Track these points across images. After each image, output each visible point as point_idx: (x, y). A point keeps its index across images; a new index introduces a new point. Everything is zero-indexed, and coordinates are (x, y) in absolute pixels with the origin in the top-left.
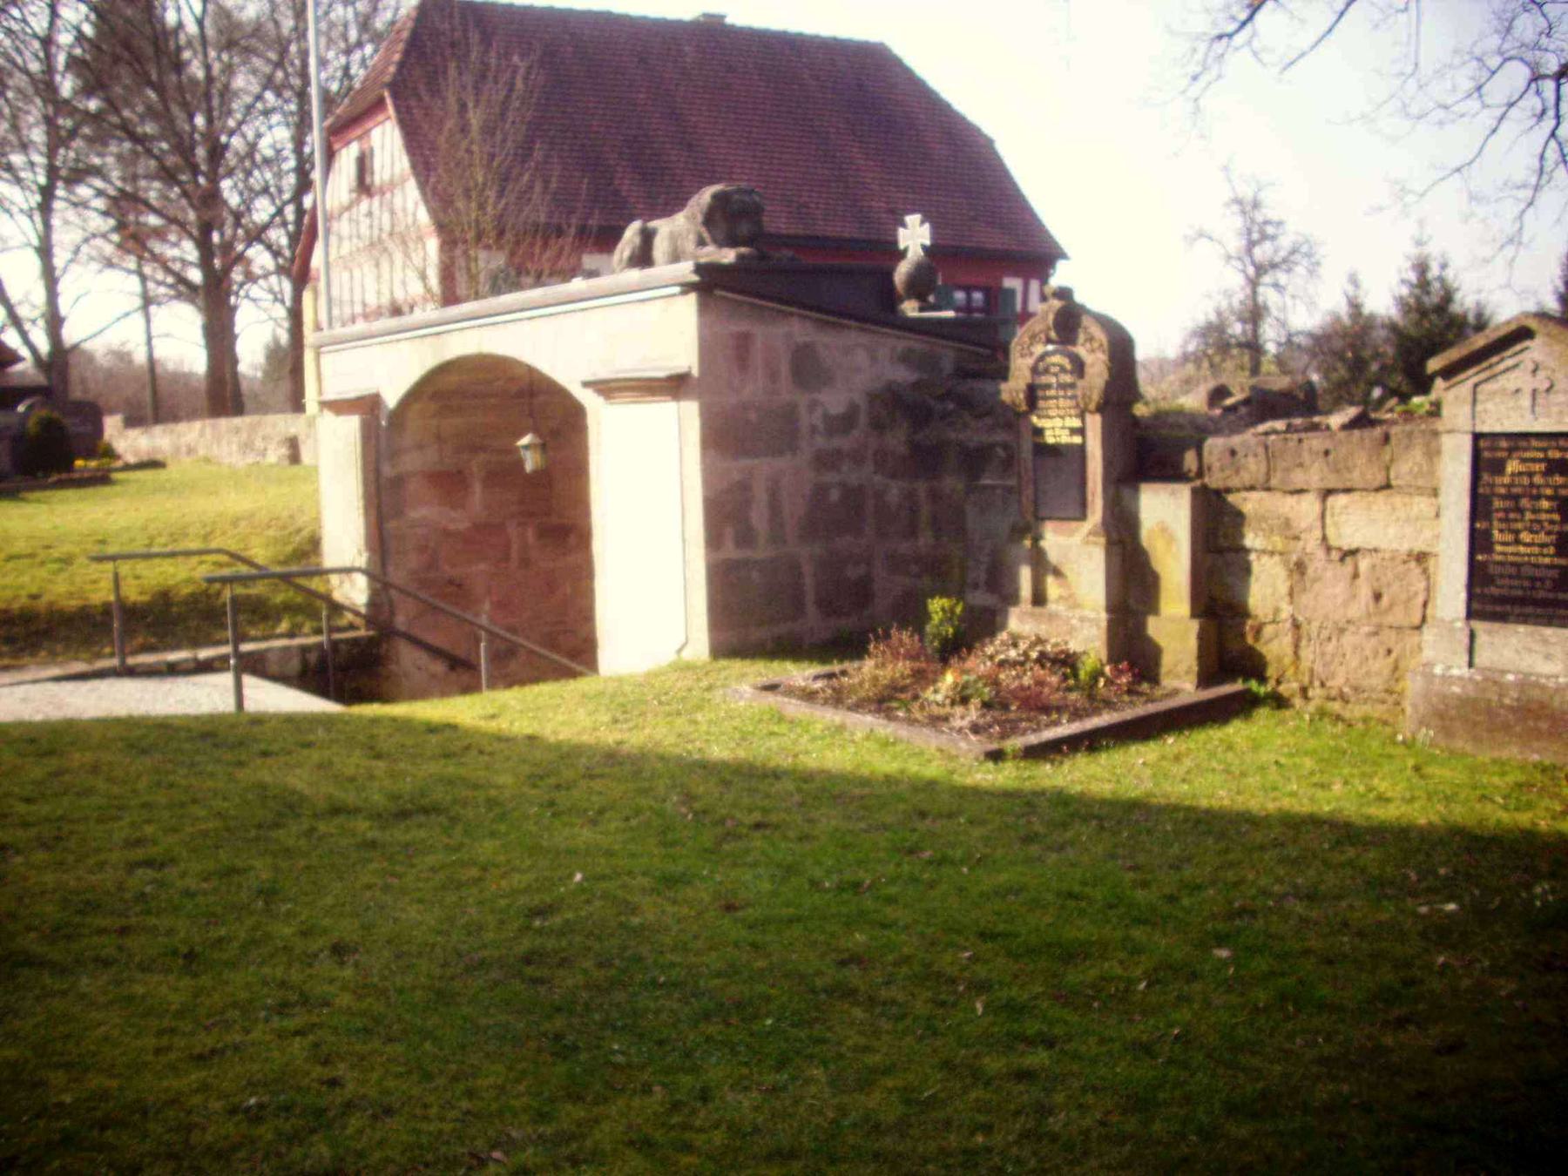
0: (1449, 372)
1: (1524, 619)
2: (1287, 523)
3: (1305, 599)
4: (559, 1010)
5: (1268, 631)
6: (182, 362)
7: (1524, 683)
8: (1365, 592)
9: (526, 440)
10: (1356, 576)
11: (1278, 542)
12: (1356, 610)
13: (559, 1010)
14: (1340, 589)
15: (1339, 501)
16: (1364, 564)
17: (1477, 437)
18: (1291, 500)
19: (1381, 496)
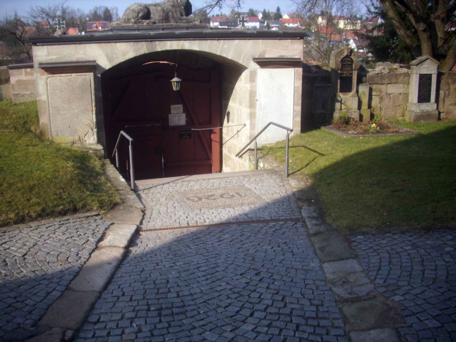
0: (53, 69)
1: (425, 102)
2: (380, 90)
3: (383, 103)
4: (206, 294)
5: (375, 110)
6: (291, 43)
7: (427, 111)
8: (392, 100)
9: (175, 79)
10: (390, 98)
11: (379, 93)
12: (391, 104)
13: (206, 294)
14: (388, 101)
15: (389, 85)
16: (392, 96)
17: (420, 74)
18: (381, 86)
19: (395, 85)
